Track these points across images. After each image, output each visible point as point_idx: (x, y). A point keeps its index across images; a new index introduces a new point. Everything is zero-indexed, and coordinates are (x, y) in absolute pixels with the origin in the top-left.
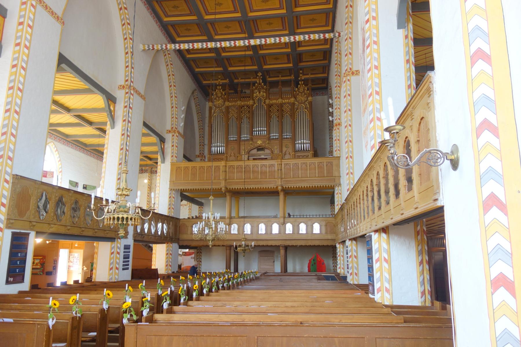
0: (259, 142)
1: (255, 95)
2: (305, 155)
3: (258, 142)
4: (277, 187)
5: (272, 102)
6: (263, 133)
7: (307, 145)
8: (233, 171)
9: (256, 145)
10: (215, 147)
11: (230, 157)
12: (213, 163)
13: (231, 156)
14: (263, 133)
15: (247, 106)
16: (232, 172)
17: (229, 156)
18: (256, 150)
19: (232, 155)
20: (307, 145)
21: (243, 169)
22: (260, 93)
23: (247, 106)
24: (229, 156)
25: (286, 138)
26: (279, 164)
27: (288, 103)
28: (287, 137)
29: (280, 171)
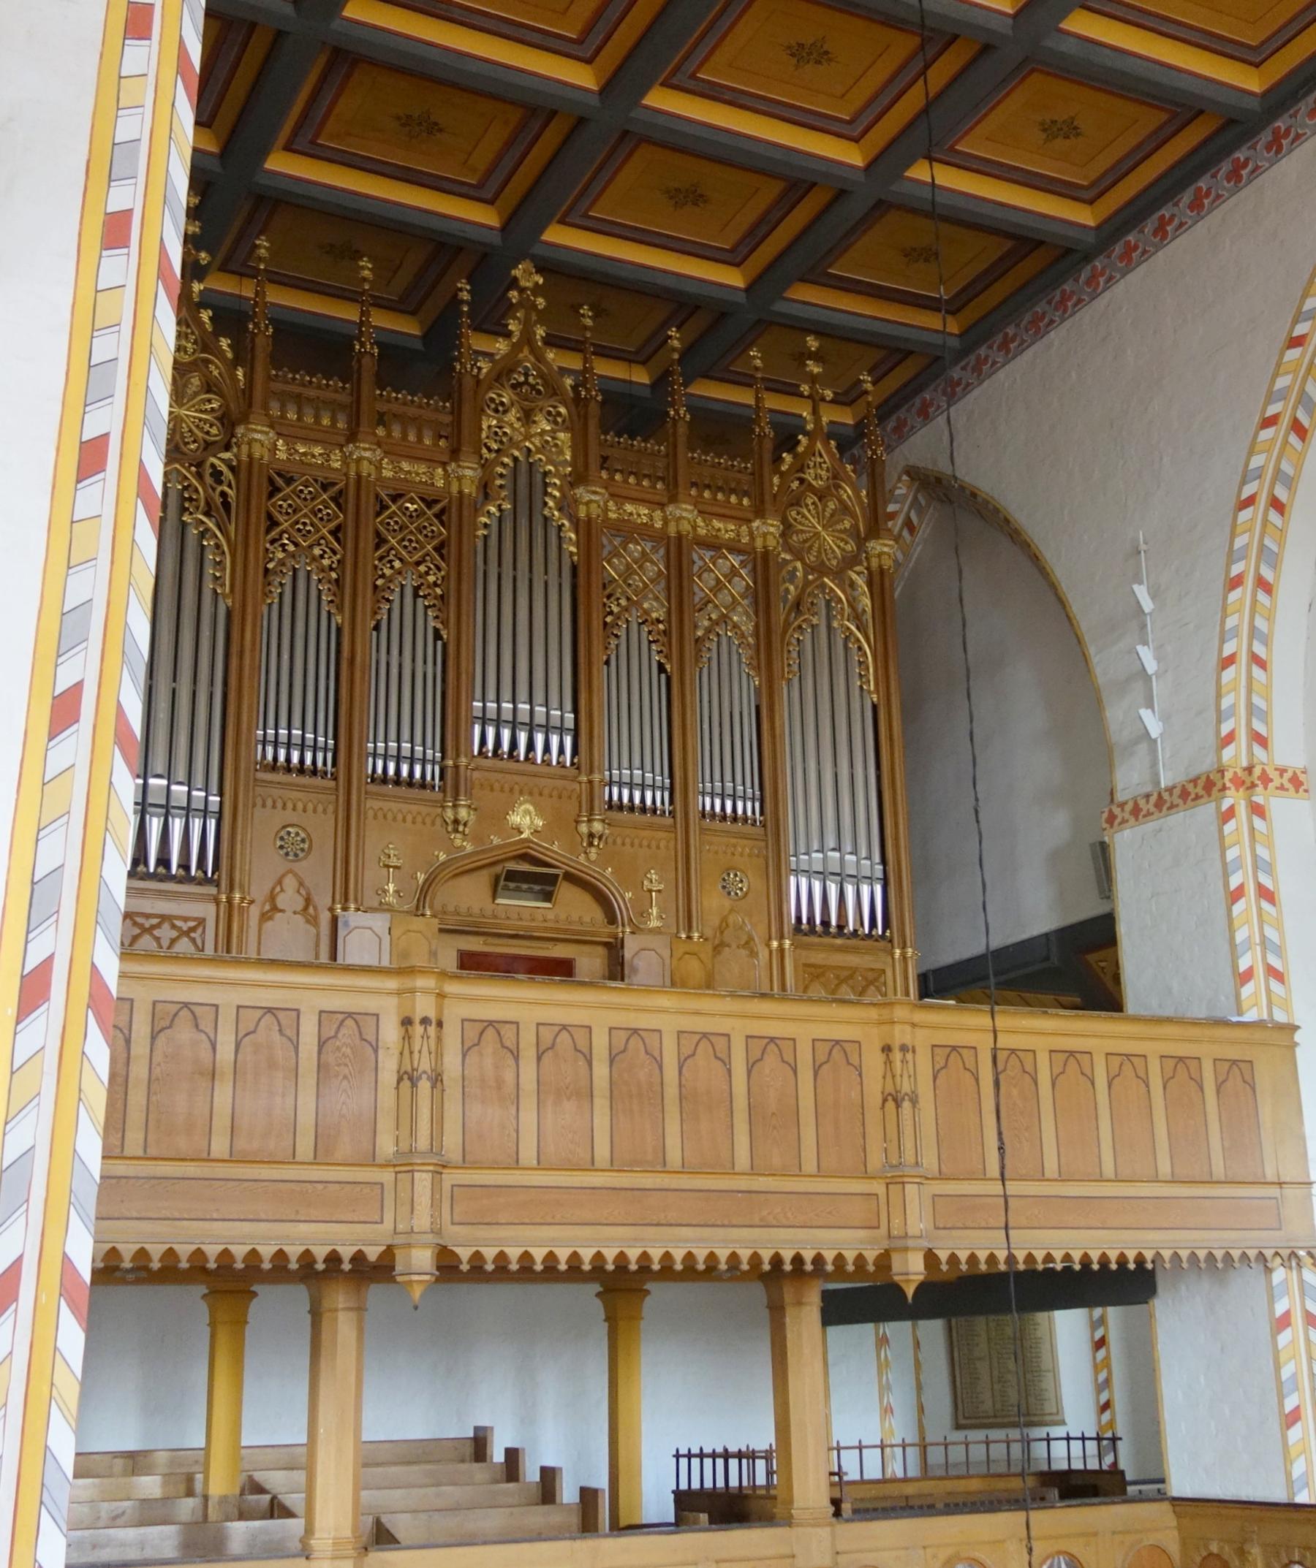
0: (525, 819)
1: (489, 422)
2: (164, 918)
3: (515, 819)
4: (884, 1261)
5: (291, 450)
6: (547, 749)
7: (196, 824)
8: (509, 1076)
9: (496, 841)
10: (823, 875)
11: (265, 917)
12: (1001, 1022)
13: (275, 909)
14: (547, 749)
15: (325, 487)
16: (500, 1084)
17: (255, 912)
18: (482, 881)
19: (289, 898)
20: (196, 824)
21: (601, 1070)
22: (527, 418)
23: (429, 504)
24: (255, 912)
25: (397, 781)
26: (425, 1021)
27: (644, 532)
28: (282, 753)
29: (424, 1085)
